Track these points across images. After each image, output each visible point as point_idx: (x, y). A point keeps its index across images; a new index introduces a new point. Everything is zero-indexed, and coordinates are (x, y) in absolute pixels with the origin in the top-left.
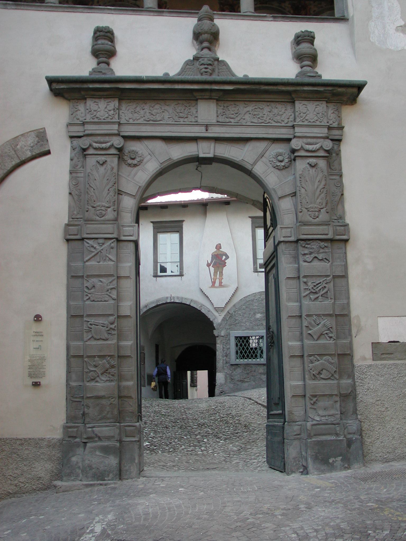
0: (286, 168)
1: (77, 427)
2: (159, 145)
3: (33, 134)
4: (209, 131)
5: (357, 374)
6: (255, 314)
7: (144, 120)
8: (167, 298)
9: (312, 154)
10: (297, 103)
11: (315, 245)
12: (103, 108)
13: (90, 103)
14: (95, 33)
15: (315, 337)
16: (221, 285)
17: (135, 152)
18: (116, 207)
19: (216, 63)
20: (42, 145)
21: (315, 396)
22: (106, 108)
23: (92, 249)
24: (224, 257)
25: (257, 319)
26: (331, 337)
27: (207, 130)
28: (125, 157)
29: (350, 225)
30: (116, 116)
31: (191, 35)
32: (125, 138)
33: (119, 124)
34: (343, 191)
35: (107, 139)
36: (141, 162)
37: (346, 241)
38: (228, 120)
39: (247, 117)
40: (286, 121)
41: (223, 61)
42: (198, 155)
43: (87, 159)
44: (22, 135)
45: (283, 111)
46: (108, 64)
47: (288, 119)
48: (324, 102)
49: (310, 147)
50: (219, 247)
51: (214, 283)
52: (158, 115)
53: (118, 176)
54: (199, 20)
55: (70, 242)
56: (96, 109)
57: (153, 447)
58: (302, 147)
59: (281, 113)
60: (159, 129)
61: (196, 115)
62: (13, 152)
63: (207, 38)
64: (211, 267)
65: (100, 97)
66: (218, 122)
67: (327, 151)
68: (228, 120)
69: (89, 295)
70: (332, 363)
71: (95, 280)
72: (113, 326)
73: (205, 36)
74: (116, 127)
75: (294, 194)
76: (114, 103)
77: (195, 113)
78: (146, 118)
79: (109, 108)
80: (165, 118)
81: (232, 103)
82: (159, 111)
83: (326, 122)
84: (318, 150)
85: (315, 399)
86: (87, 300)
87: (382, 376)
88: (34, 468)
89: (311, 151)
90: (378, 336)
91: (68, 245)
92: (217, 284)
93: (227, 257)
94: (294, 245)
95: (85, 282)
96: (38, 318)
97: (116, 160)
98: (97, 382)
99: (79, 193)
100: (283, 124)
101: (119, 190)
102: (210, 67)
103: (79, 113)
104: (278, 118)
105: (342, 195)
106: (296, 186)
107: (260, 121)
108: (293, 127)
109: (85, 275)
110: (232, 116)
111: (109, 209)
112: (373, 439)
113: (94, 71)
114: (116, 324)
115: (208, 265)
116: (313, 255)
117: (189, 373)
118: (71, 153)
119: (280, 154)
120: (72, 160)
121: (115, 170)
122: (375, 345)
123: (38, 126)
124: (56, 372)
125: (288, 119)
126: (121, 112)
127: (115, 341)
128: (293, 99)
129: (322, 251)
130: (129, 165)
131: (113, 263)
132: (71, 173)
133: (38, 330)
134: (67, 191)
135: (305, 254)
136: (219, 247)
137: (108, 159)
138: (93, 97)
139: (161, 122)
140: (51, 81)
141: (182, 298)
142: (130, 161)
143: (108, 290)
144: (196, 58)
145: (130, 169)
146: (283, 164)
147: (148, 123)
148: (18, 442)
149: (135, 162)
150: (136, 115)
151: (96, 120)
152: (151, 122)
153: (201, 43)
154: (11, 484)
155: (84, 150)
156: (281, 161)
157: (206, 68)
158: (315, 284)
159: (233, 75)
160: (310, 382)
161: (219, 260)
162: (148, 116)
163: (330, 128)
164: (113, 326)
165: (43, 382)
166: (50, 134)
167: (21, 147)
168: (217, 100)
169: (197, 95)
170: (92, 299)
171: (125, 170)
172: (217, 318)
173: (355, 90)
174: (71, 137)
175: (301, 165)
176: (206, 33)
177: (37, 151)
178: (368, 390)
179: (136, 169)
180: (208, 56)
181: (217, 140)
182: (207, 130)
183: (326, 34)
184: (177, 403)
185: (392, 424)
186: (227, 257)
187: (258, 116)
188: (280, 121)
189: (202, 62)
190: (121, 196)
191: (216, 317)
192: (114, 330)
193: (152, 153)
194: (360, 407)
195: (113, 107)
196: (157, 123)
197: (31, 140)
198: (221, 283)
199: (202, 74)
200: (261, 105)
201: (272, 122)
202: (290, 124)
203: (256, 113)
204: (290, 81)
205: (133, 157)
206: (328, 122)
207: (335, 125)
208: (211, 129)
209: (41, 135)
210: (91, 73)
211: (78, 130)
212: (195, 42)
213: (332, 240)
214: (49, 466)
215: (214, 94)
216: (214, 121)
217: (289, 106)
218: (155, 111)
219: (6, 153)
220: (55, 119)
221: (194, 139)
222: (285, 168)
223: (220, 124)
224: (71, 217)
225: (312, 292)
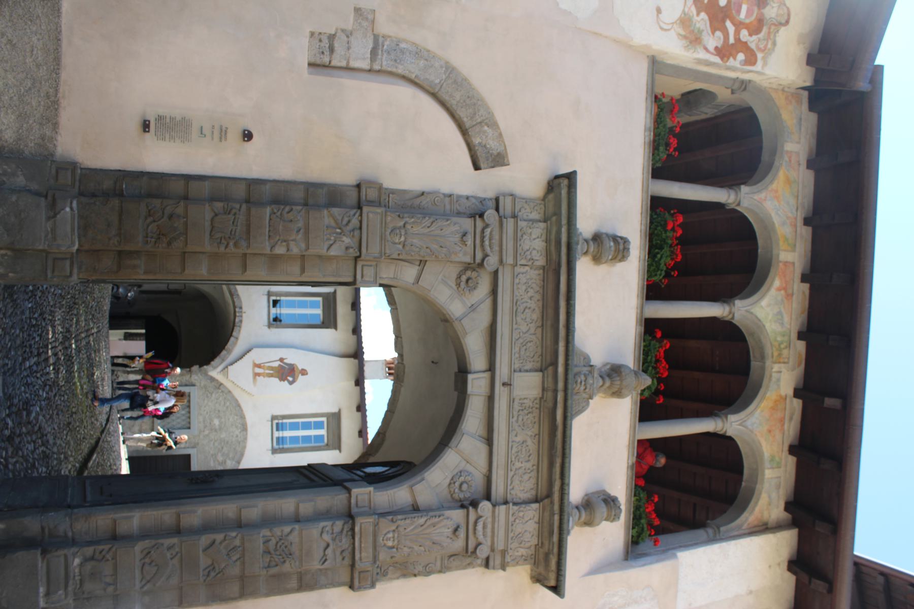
0: (450, 484)
2: (483, 317)
3: (501, 149)
6: (219, 417)
8: (241, 308)
12: (534, 243)
14: (621, 238)
16: (256, 375)
19: (587, 396)
24: (290, 379)
25: (211, 420)
29: (372, 591)
30: (523, 262)
32: (496, 273)
36: (458, 285)
37: (351, 587)
38: (515, 413)
41: (588, 404)
42: (470, 373)
43: (469, 220)
44: (500, 135)
49: (480, 527)
50: (304, 372)
51: (259, 366)
55: (356, 189)
57: (39, 294)
58: (481, 517)
60: (507, 318)
62: (479, 120)
64: (279, 363)
68: (515, 413)
76: (541, 261)
80: (520, 329)
81: (537, 419)
89: (475, 529)
91: (353, 186)
92: (258, 370)
93: (291, 383)
97: (468, 259)
99: (415, 207)
105: (415, 575)
110: (520, 419)
115: (281, 360)
117: (143, 331)
123: (511, 156)
124: (161, 157)
127: (208, 248)
128: (542, 500)
132: (450, 196)
133: (229, 135)
136: (304, 372)
140: (571, 177)
141: (240, 327)
142: (464, 278)
145: (454, 276)
147: (514, 303)
151: (519, 234)
155: (481, 216)
161: (287, 373)
167: (485, 132)
168: (541, 398)
171: (452, 271)
172: (214, 371)
173: (552, 583)
174: (497, 200)
181: (491, 399)
183: (612, 533)
184: (106, 321)
186: (291, 383)
190: (418, 263)
191: (215, 368)
192: (226, 247)
193: (473, 308)
195: (535, 258)
197: (493, 144)
198: (259, 375)
201: (512, 473)
204: (566, 497)
207: (508, 559)
209: (499, 160)
212: (608, 367)
213: (353, 566)
215: (550, 394)
219: (479, 110)
220: (523, 178)
221: (491, 368)
223: (511, 401)
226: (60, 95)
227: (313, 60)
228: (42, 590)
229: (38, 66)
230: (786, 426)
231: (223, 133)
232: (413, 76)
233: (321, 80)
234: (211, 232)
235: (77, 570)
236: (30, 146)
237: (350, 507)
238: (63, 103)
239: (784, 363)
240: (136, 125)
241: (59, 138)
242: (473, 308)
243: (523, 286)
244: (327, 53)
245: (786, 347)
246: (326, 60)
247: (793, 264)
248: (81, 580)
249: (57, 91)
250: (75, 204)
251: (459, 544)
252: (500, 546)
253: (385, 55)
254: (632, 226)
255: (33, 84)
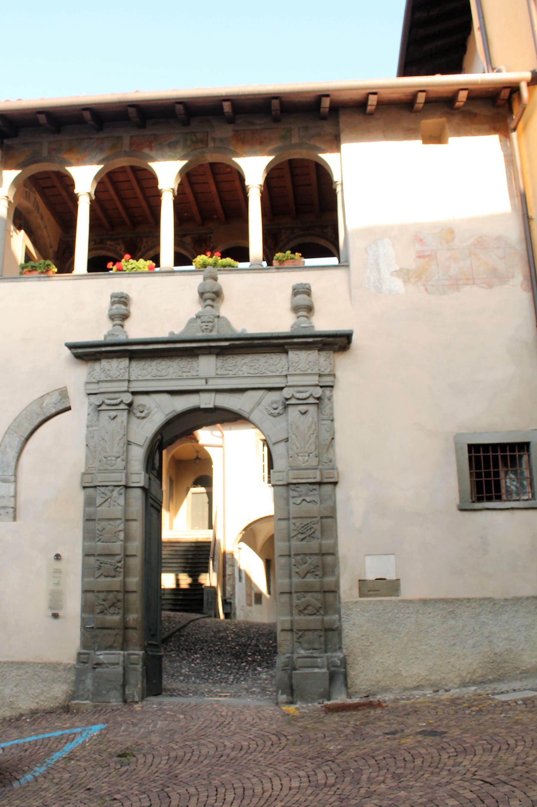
0: (281, 415)
1: (88, 654)
3: (57, 393)
4: (209, 384)
5: (343, 611)
7: (152, 376)
9: (303, 402)
10: (290, 353)
11: (303, 489)
12: (116, 367)
13: (104, 363)
15: (302, 575)
17: (144, 406)
18: (125, 456)
20: (64, 402)
21: (300, 630)
22: (118, 367)
23: (103, 495)
26: (317, 575)
27: (207, 383)
28: (135, 411)
30: (127, 374)
31: (197, 295)
32: (134, 393)
33: (129, 381)
34: (334, 434)
35: (117, 395)
36: (148, 414)
37: (335, 483)
38: (226, 372)
39: (245, 368)
40: (280, 371)
44: (48, 394)
45: (278, 360)
46: (122, 326)
47: (283, 368)
48: (316, 352)
52: (164, 371)
53: (127, 429)
54: (205, 279)
56: (108, 368)
58: (293, 395)
59: (275, 363)
61: (198, 369)
63: (212, 296)
65: (112, 358)
66: (217, 374)
67: (318, 399)
69: (100, 537)
70: (317, 600)
71: (104, 523)
72: (119, 565)
73: (207, 295)
74: (126, 383)
75: (287, 440)
76: (125, 362)
77: (196, 367)
78: (153, 374)
79: (120, 367)
82: (164, 367)
83: (317, 370)
84: (308, 398)
85: (300, 633)
86: (98, 541)
87: (368, 612)
88: (53, 688)
90: (365, 574)
94: (285, 488)
95: (97, 524)
96: (58, 557)
97: (125, 413)
98: (105, 614)
100: (278, 374)
101: (129, 441)
102: (210, 324)
103: (95, 372)
104: (273, 368)
106: (288, 433)
107: (256, 372)
108: (286, 376)
109: (97, 519)
110: (230, 368)
111: (119, 460)
112: (357, 672)
113: (110, 334)
114: (122, 563)
116: (301, 499)
118: (88, 409)
119: (275, 402)
120: (89, 415)
121: (125, 423)
122: (362, 582)
123: (61, 386)
124: (73, 605)
125: (283, 368)
126: (131, 369)
129: (310, 493)
130: (138, 418)
131: (120, 508)
132: (88, 427)
134: (84, 444)
135: (293, 497)
137: (118, 413)
138: (107, 358)
139: (166, 377)
140: (71, 347)
143: (116, 532)
144: (198, 317)
145: (139, 421)
146: (277, 411)
148: (40, 666)
149: (143, 415)
150: (144, 372)
151: (109, 379)
152: (157, 378)
153: (205, 300)
154: (33, 702)
156: (276, 409)
157: (206, 326)
158: (302, 525)
159: (232, 330)
160: (297, 618)
162: (155, 372)
163: (320, 375)
164: (119, 565)
165: (60, 614)
166: (71, 392)
167: (47, 405)
169: (198, 352)
170: (102, 540)
175: (294, 412)
176: (209, 292)
177: (60, 408)
178: (354, 625)
179: (145, 420)
180: (209, 314)
182: (207, 383)
185: (376, 658)
187: (254, 367)
188: (275, 371)
189: (203, 320)
190: (130, 446)
192: (120, 568)
193: (158, 406)
194: (346, 641)
196: (162, 378)
197: (56, 397)
199: (203, 331)
200: (257, 357)
202: (284, 373)
203: (252, 364)
205: (141, 410)
206: (319, 370)
208: (210, 382)
209: (64, 393)
210: (105, 337)
211: (94, 388)
214: (65, 687)
215: (213, 351)
216: (213, 374)
217: (283, 356)
218: (161, 367)
220: (76, 378)
222: (279, 414)
224: (88, 467)
225: (300, 533)
226: (41, 661)
227: (12, 519)
228: (316, 670)
229: (27, 672)
230: (258, 127)
231: (57, 571)
232: (17, 455)
233: (21, 513)
234: (406, 714)
235: (308, 652)
236: (72, 677)
237: (283, 485)
238: (45, 660)
239: (207, 136)
240: (56, 622)
241: (64, 662)
242: (158, 406)
243: (145, 373)
244: (7, 510)
245: (195, 136)
246: (11, 510)
247: (131, 137)
248: (314, 649)
249: (39, 663)
250: (98, 653)
251: (312, 410)
252: (315, 380)
253: (6, 474)
254: (107, 285)
255: (37, 675)
